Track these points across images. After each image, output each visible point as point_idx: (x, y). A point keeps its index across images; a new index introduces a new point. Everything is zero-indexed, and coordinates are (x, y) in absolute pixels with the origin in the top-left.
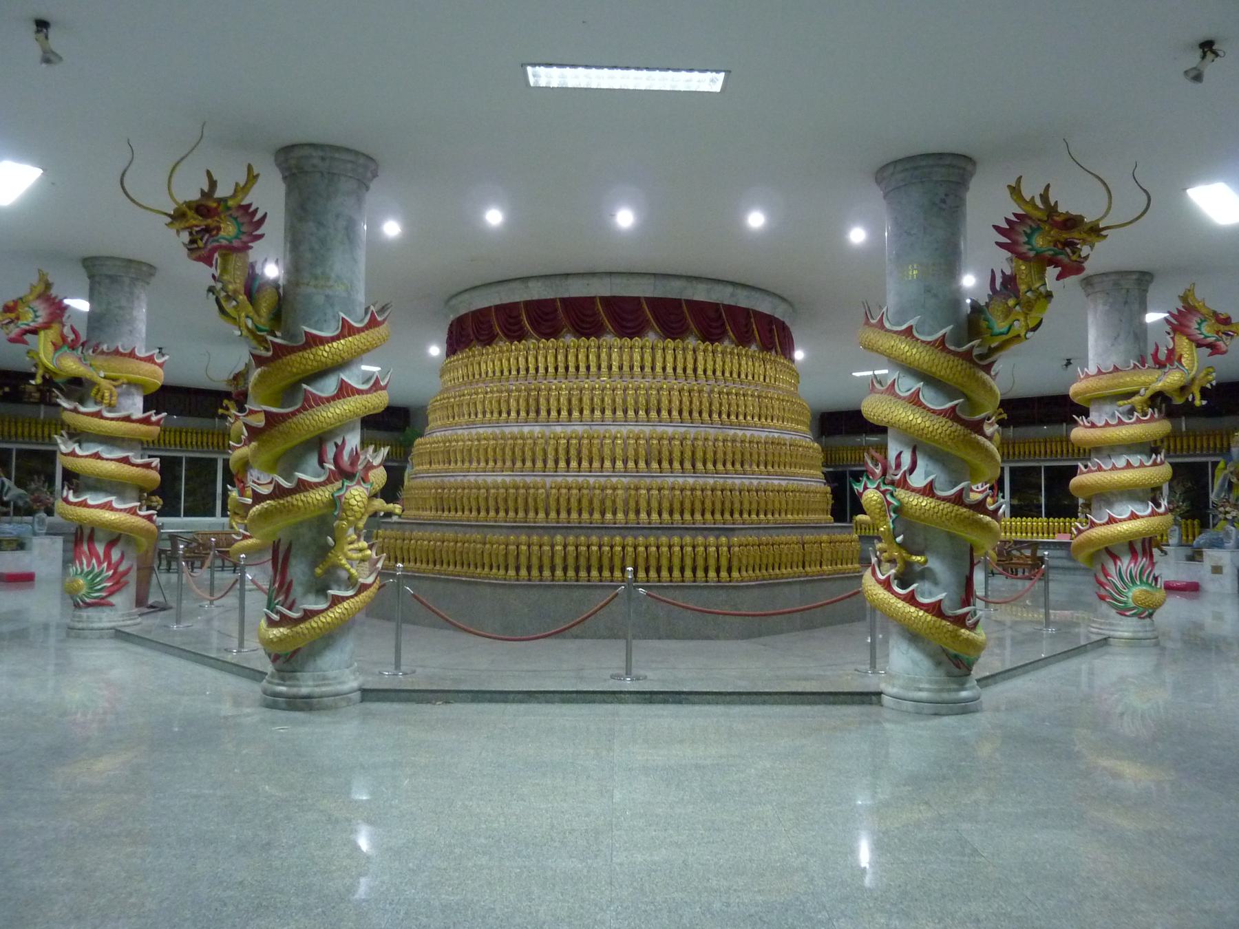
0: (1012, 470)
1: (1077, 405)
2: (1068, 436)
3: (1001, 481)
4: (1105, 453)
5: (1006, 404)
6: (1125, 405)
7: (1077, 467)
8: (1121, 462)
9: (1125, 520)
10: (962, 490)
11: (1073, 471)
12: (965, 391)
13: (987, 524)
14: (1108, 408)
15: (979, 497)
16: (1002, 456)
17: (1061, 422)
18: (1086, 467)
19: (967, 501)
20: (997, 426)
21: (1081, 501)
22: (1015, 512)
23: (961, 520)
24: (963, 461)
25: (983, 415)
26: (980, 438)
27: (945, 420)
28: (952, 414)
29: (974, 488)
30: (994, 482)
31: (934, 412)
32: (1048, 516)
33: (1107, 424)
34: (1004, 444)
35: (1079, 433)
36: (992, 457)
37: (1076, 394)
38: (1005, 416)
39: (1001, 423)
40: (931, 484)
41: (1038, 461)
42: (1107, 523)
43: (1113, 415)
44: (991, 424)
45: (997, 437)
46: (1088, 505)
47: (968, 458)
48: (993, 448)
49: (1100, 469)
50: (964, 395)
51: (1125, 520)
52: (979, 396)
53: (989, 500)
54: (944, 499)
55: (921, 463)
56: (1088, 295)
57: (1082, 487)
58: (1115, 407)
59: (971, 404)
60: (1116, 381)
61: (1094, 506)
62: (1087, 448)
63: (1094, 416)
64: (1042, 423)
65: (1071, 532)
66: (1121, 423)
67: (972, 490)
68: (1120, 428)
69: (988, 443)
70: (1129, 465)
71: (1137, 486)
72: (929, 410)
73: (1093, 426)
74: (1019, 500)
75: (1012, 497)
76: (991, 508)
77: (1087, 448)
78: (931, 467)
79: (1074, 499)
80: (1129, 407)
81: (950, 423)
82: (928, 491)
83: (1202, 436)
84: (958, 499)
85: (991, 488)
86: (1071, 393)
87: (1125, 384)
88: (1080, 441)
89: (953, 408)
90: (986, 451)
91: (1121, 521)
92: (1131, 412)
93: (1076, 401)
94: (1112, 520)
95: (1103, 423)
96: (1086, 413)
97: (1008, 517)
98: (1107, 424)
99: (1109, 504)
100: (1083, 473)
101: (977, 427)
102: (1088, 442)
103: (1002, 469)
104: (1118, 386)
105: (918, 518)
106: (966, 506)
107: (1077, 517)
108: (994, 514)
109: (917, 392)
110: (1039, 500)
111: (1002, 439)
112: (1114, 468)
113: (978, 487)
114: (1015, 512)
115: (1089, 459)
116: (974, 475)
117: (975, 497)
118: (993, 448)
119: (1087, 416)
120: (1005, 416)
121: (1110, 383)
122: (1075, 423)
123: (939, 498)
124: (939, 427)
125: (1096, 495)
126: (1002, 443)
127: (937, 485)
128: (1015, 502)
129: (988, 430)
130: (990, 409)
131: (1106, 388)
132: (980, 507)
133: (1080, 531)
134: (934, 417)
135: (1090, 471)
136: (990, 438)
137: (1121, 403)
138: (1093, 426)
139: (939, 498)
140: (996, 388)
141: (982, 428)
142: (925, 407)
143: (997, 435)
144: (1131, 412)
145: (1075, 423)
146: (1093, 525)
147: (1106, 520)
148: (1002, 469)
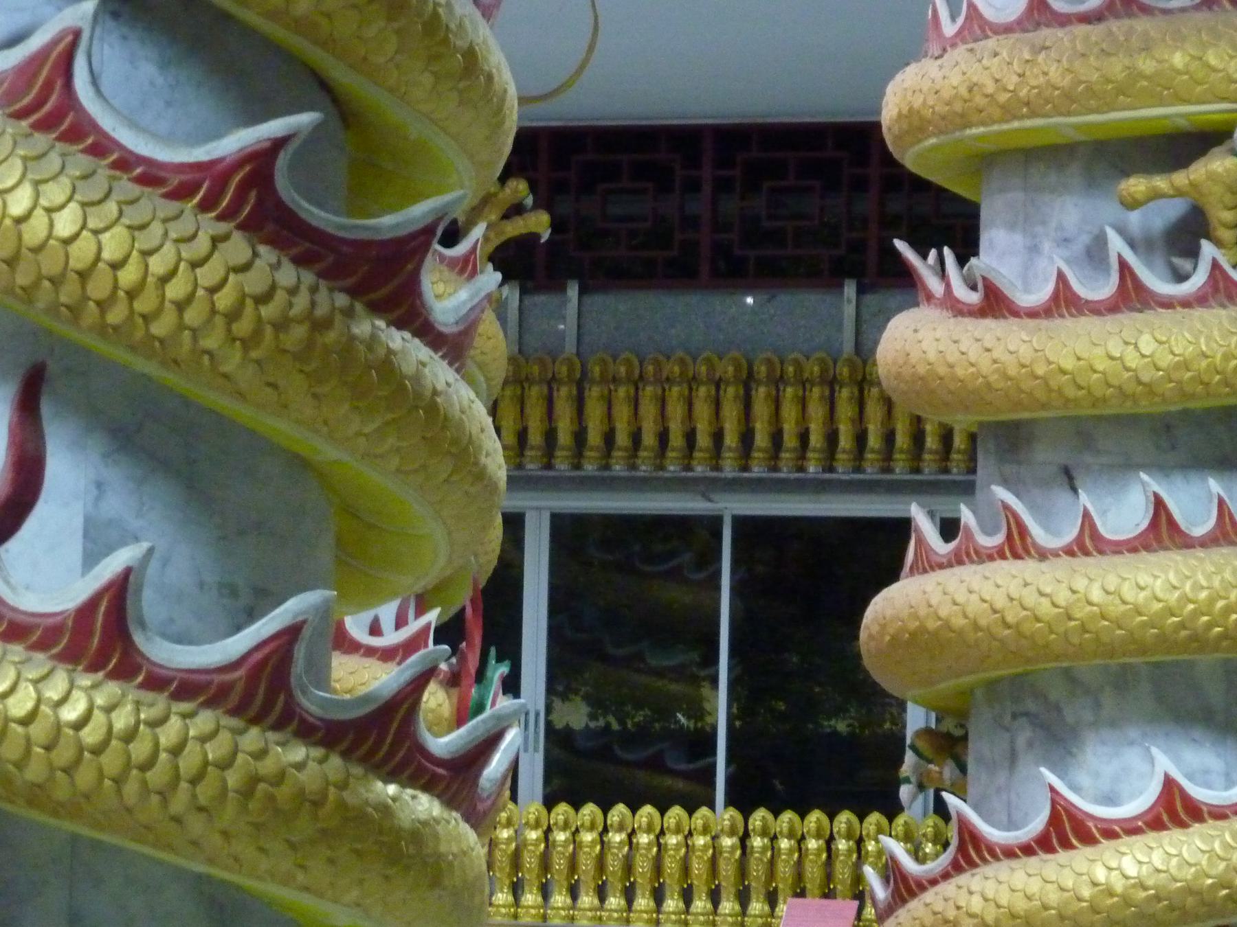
0: (568, 531)
1: (920, 185)
2: (864, 351)
3: (501, 593)
4: (1045, 455)
5: (553, 156)
6: (1157, 196)
7: (901, 528)
8: (1123, 510)
9: (1131, 828)
10: (292, 633)
11: (879, 552)
12: (339, 74)
13: (420, 834)
14: (1072, 210)
15: (381, 679)
16: (518, 447)
17: (828, 276)
18: (949, 529)
19: (311, 702)
20: (490, 278)
21: (916, 719)
22: (577, 773)
23: (272, 810)
24: (300, 464)
25: (419, 212)
26: (397, 339)
27: (209, 226)
28: (250, 198)
29: (356, 627)
30: (463, 597)
31: (151, 176)
32: (742, 800)
33: (1064, 301)
34: (529, 383)
35: (923, 341)
36: (462, 453)
37: (916, 124)
38: (539, 223)
39: (514, 260)
40: (120, 591)
41: (708, 486)
42: (1043, 844)
43: (1096, 253)
44: (466, 268)
45: (493, 342)
46: (949, 745)
47: (326, 452)
48: (466, 401)
49: (1017, 544)
50: (325, 91)
51: (1131, 828)
52: (406, 103)
53: (435, 699)
54: (188, 688)
55: (68, 471)
56: (169, 104)
57: (925, 642)
58: (1108, 210)
59: (360, 143)
60: (1117, 67)
61: (978, 748)
62: (962, 423)
63: (1000, 253)
64: (733, 272)
65: (860, 895)
66: (1131, 295)
67: (345, 644)
68: (1128, 321)
69: (439, 373)
70: (1163, 530)
71: (1198, 641)
72: (125, 162)
73: (995, 303)
74: (597, 704)
75: (560, 679)
76: (443, 743)
77: (962, 423)
78: (116, 505)
79: (879, 703)
80: (1173, 210)
81: (238, 248)
82: (101, 636)
83: (778, 381)
84: (265, 691)
85: (450, 632)
86: (888, 115)
87: (1164, 87)
88: (925, 385)
89: (260, 162)
90: (429, 413)
91: (1109, 833)
92: (1187, 234)
93: (911, 158)
94: (1066, 830)
95: (1041, 294)
96: (957, 229)
97: (532, 807)
98: (1064, 301)
99: (1059, 740)
100: (929, 564)
101: (384, 277)
102: (968, 395)
103: (514, 524)
104: (1125, 90)
105: (36, 795)
106: (307, 731)
107: (892, 809)
108: (456, 779)
109: (62, 58)
110: (698, 711)
111: (520, 356)
112: (1090, 542)
113: (381, 620)
114: (577, 773)
115: (967, 489)
116: (360, 552)
117: (359, 679)
118: (466, 401)
119: (967, 248)
120: (539, 223)
121: (1090, 72)
122: (902, 281)
123: (156, 682)
124: (178, 265)
125: (992, 686)
126: (518, 380)
127: (150, 603)
128: (576, 715)
129: (449, 295)
130: (459, 175)
131: (1069, 100)
132: (381, 736)
133: (905, 889)
134: (152, 204)
135: (968, 555)
136: (453, 346)
137: (1137, 185)
138: (995, 303)
139: (156, 682)
140: (497, 60)
141: (412, 288)
142: (101, 147)
143: (489, 326)
144: (1187, 234)
145: (902, 281)
146: (971, 851)
147: (1037, 824)
148: (514, 524)
